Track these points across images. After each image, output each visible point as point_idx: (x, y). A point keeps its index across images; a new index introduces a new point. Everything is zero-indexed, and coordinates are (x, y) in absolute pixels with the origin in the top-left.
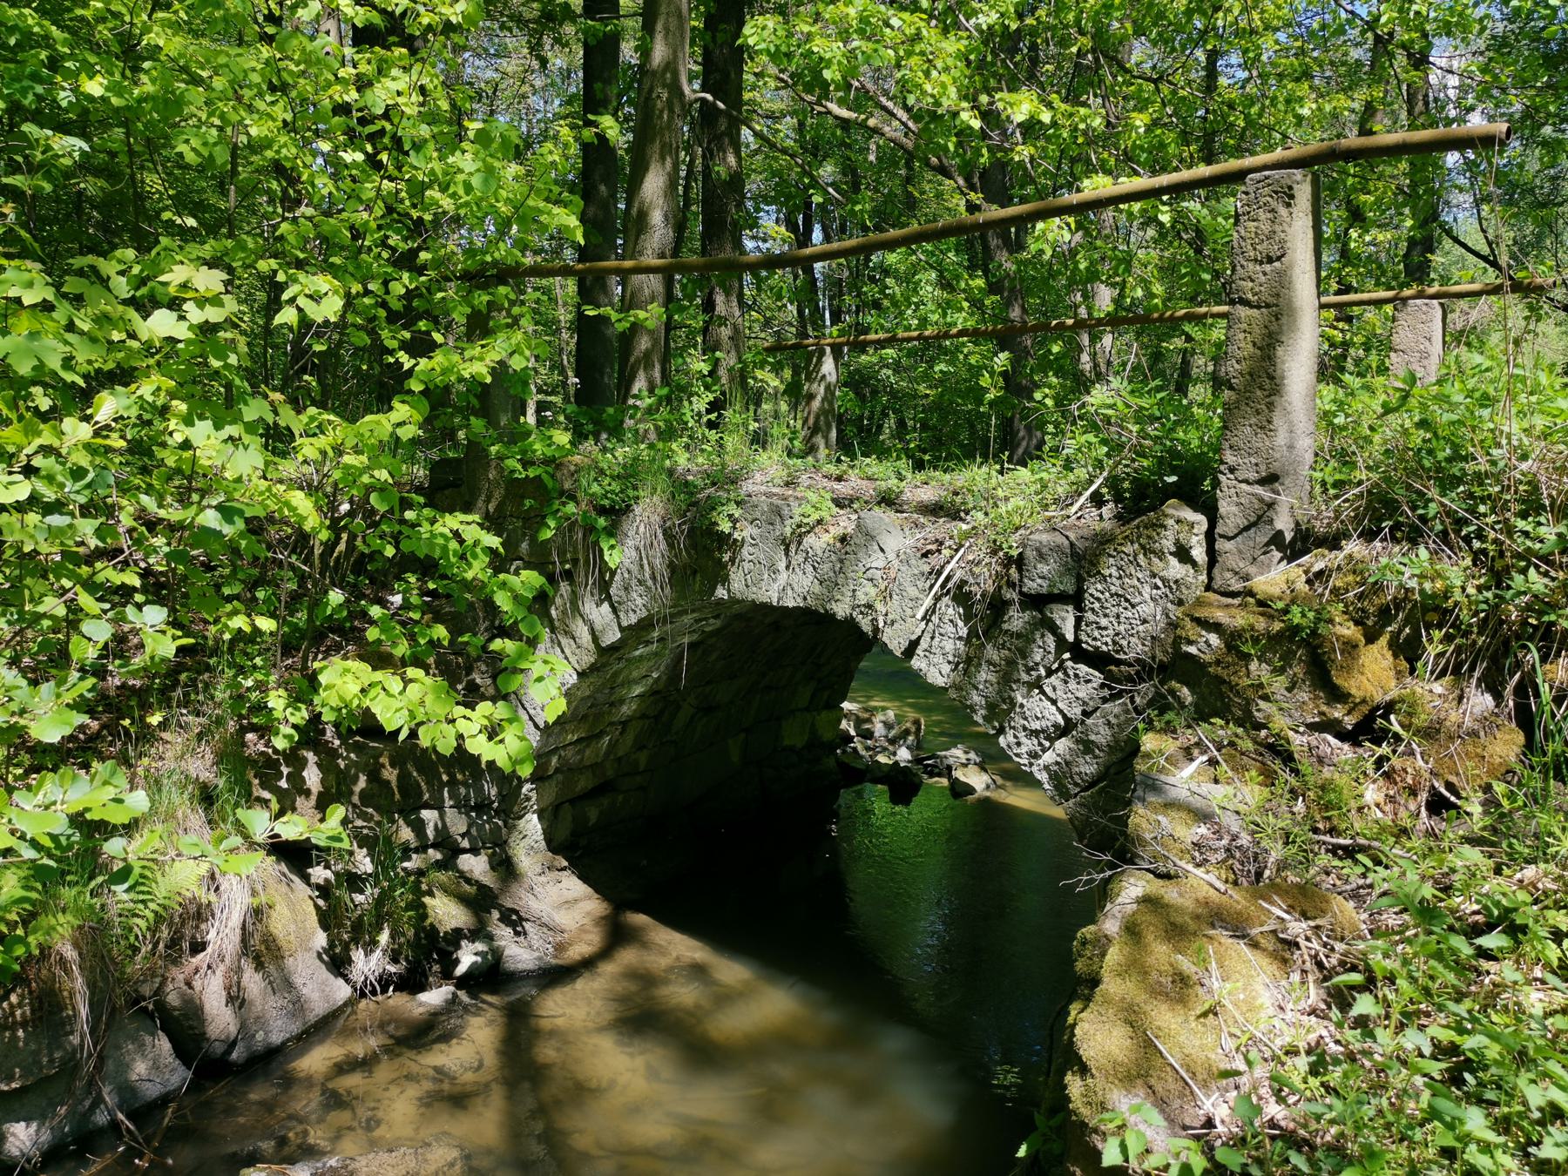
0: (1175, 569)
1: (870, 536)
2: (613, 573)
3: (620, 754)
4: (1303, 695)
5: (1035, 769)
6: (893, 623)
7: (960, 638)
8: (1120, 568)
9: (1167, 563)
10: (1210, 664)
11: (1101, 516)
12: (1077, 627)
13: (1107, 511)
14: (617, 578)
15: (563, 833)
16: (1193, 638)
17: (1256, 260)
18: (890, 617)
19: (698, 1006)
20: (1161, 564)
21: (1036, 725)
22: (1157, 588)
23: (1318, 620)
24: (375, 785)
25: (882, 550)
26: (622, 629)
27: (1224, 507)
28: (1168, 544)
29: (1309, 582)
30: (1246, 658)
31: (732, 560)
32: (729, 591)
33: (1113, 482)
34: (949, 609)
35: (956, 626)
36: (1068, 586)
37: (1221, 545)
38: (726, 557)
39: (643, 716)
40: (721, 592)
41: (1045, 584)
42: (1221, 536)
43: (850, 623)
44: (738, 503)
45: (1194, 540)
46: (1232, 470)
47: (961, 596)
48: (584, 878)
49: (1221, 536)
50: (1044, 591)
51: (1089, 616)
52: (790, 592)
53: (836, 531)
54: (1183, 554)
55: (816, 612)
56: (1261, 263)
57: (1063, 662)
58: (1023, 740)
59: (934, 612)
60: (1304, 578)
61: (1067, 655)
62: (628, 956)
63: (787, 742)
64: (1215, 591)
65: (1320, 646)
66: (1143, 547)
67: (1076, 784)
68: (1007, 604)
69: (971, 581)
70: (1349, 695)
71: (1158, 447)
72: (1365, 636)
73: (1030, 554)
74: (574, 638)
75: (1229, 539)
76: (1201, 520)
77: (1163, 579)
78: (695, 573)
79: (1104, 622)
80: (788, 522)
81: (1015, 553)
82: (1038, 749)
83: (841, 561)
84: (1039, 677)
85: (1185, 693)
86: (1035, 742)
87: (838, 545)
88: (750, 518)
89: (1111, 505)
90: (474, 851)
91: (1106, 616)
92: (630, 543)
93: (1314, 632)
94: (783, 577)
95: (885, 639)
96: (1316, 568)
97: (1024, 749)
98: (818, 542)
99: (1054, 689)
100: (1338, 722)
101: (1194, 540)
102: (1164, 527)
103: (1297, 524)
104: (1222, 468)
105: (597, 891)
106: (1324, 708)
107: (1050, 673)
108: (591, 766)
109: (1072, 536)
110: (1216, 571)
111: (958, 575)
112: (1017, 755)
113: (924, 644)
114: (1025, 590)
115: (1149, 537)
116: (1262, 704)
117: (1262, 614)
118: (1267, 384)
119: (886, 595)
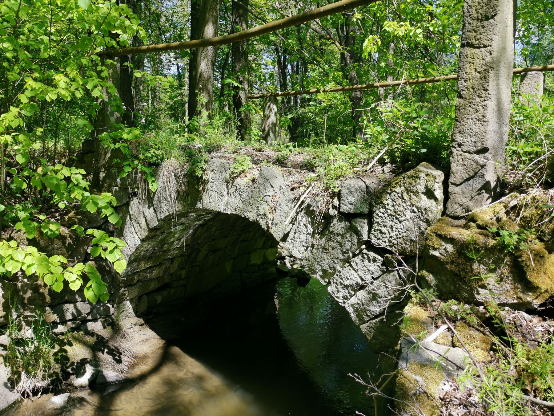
0: (425, 202)
1: (266, 179)
2: (154, 194)
3: (172, 272)
4: (508, 286)
5: (346, 305)
6: (276, 224)
7: (309, 234)
8: (393, 201)
9: (420, 198)
10: (447, 263)
11: (383, 171)
12: (369, 232)
13: (387, 168)
14: (156, 196)
15: (143, 307)
16: (436, 246)
17: (478, 19)
18: (275, 221)
19: (190, 403)
20: (416, 199)
21: (347, 283)
22: (414, 212)
23: (520, 240)
24: (36, 294)
25: (272, 186)
26: (158, 221)
27: (455, 167)
28: (421, 187)
29: (507, 213)
30: (471, 261)
31: (204, 190)
32: (202, 205)
33: (391, 153)
34: (303, 219)
35: (306, 227)
36: (366, 210)
37: (452, 189)
38: (201, 188)
39: (182, 256)
40: (199, 205)
41: (352, 207)
42: (452, 184)
43: (256, 224)
44: (206, 162)
45: (436, 185)
46: (460, 145)
47: (309, 212)
48: (153, 329)
49: (452, 184)
50: (352, 211)
51: (376, 226)
52: (229, 206)
53: (250, 176)
54: (430, 194)
55: (241, 217)
56: (481, 20)
57: (362, 250)
58: (341, 290)
59: (296, 219)
60: (504, 210)
61: (364, 247)
62: (167, 371)
63: (253, 262)
64: (448, 216)
65: (520, 256)
66: (406, 189)
67: (368, 316)
68: (331, 218)
69: (314, 204)
70: (538, 287)
71: (416, 133)
72: (547, 248)
73: (344, 191)
74: (139, 223)
75: (457, 185)
76: (440, 175)
77: (418, 208)
78: (188, 195)
79: (384, 230)
80: (228, 171)
81: (336, 190)
82: (348, 295)
83: (252, 192)
84: (349, 257)
85: (430, 278)
86: (347, 291)
87: (251, 183)
88: (211, 169)
89: (389, 165)
90: (95, 320)
91: (385, 226)
92: (161, 180)
93: (517, 248)
94: (225, 199)
95: (272, 232)
96: (512, 204)
97: (340, 295)
98: (241, 182)
99: (357, 264)
100: (529, 303)
101: (436, 185)
102: (419, 178)
103: (498, 178)
104: (454, 144)
105: (158, 335)
106: (521, 295)
107: (354, 255)
108: (157, 278)
109: (368, 182)
110: (449, 204)
111: (307, 201)
112: (337, 297)
113: (291, 236)
114: (341, 210)
115: (410, 184)
116: (481, 291)
117: (481, 234)
118: (483, 94)
119: (274, 210)
